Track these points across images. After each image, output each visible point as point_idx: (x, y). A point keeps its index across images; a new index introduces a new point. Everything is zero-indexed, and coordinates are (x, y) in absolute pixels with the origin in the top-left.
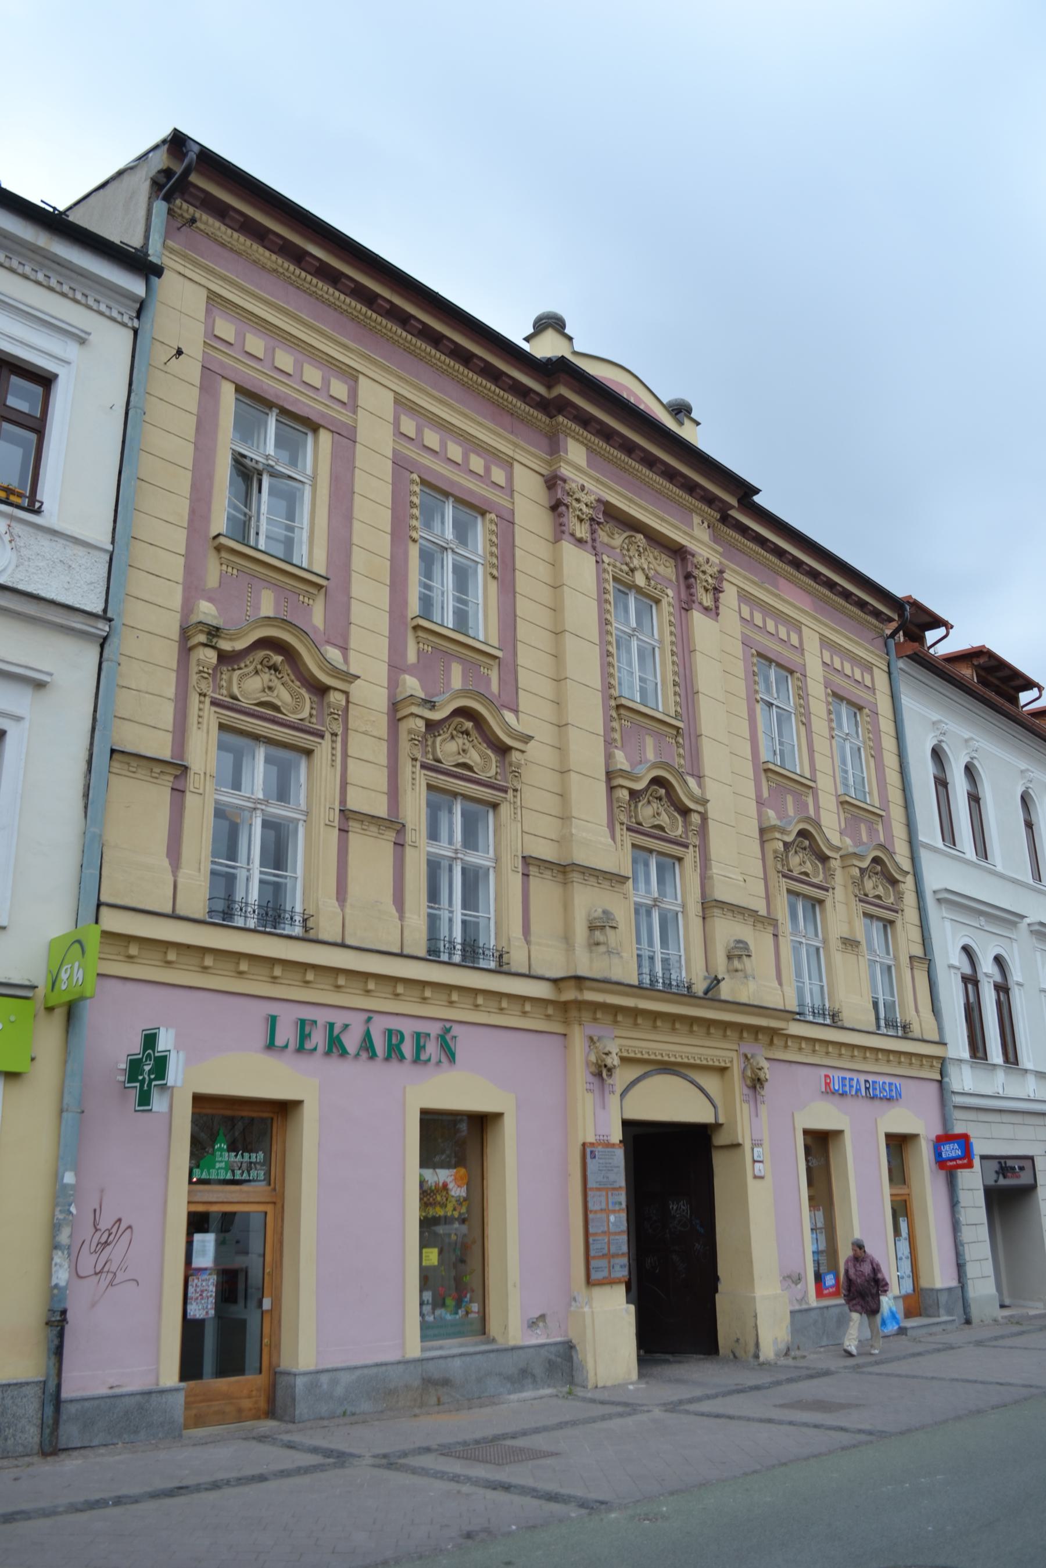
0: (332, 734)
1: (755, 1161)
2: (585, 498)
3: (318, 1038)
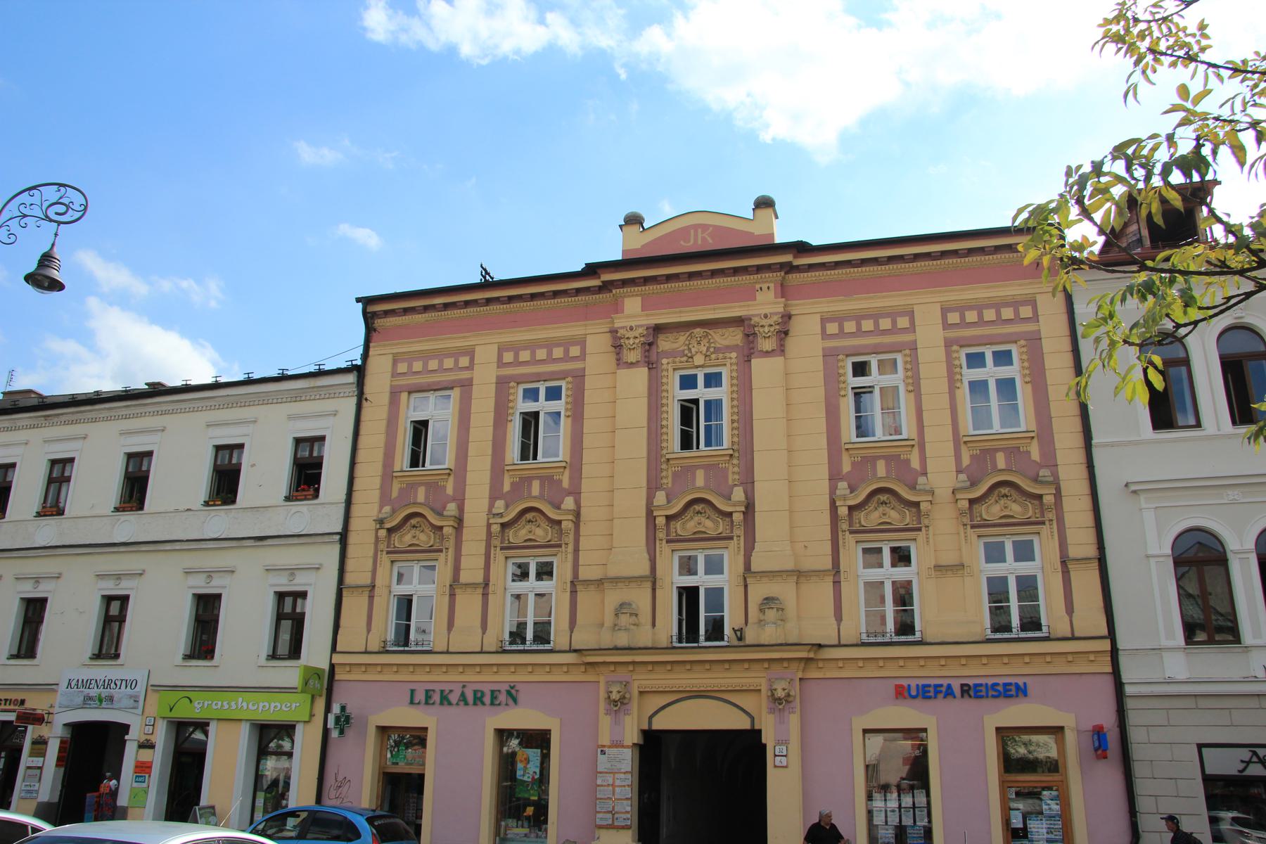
0: (737, 536)
1: (776, 756)
2: (771, 321)
3: (437, 698)
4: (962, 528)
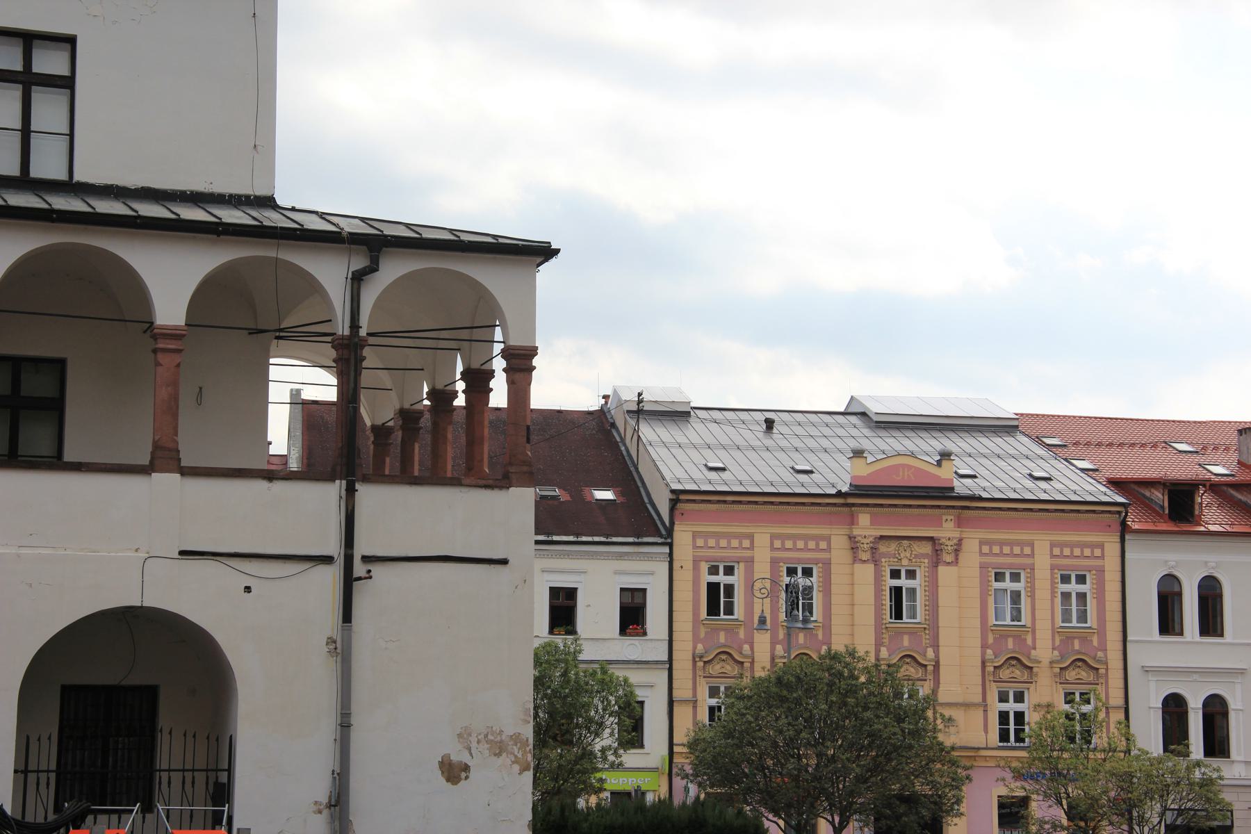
4: (1054, 683)
